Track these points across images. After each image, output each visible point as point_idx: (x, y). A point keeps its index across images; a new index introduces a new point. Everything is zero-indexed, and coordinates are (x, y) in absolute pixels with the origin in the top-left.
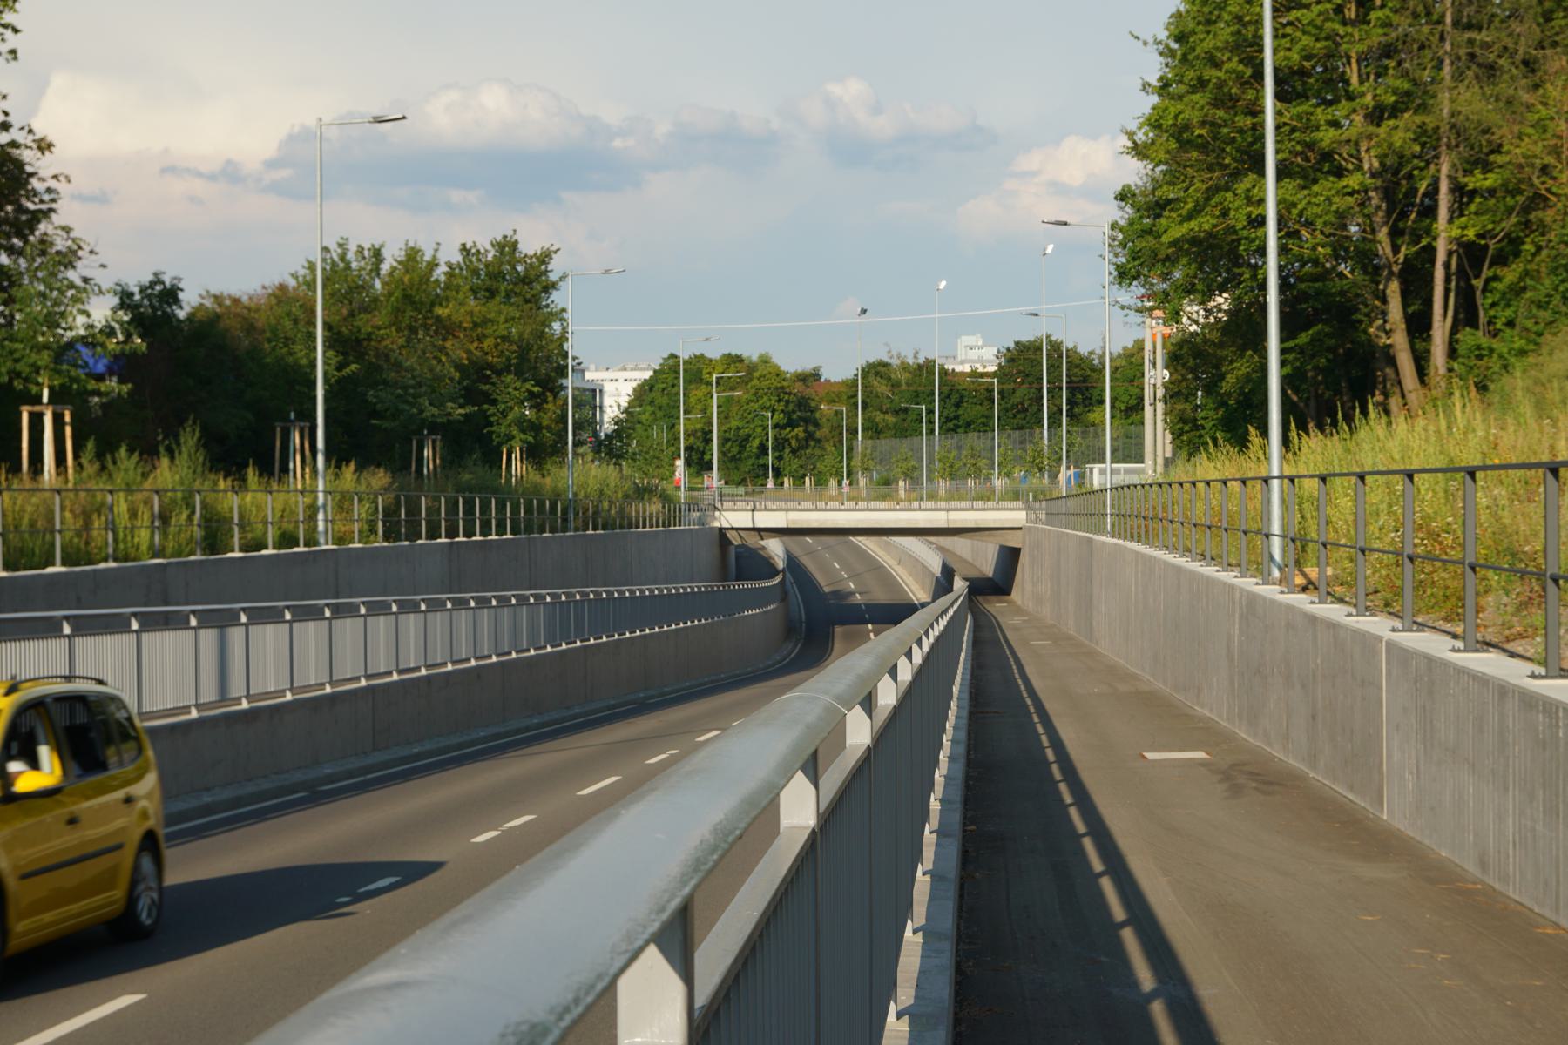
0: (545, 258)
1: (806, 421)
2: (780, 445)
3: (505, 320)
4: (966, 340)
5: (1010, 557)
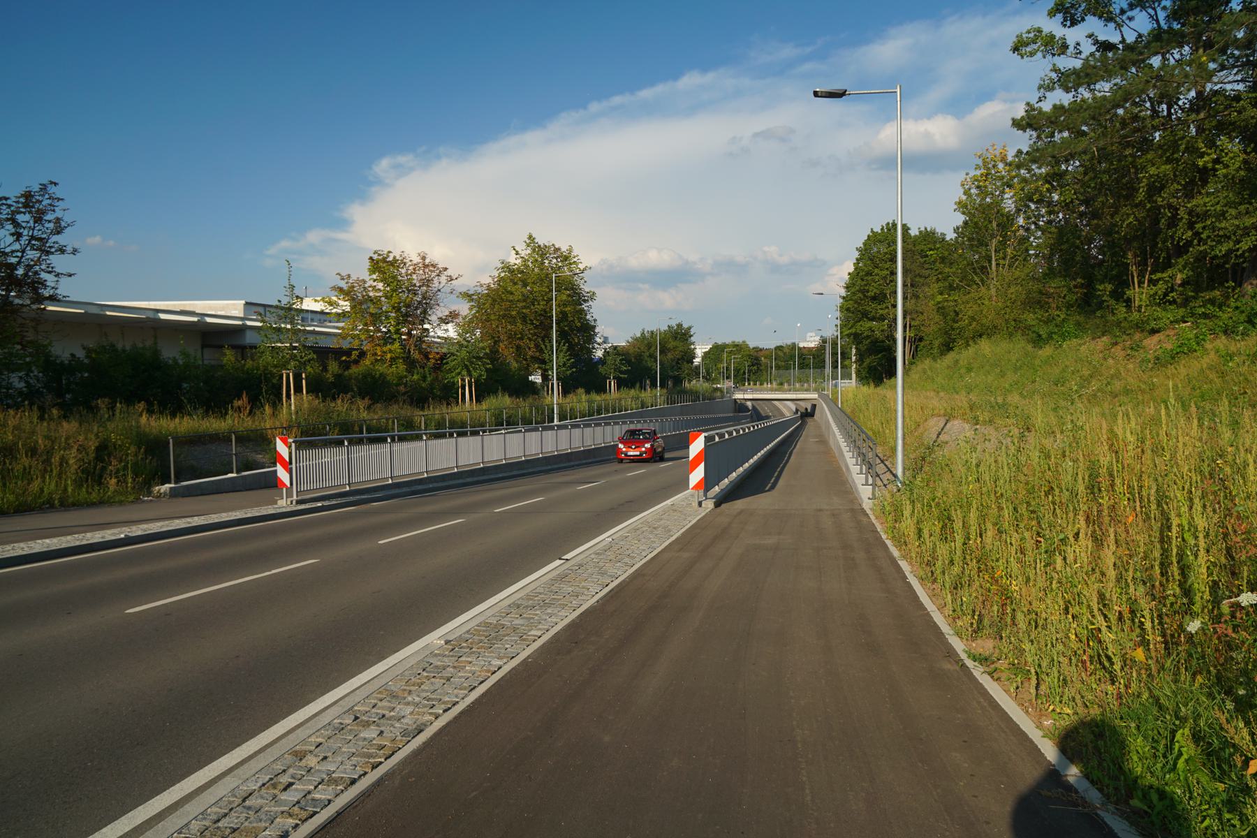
0: (690, 328)
1: (757, 364)
2: (750, 371)
4: (810, 334)
5: (814, 406)
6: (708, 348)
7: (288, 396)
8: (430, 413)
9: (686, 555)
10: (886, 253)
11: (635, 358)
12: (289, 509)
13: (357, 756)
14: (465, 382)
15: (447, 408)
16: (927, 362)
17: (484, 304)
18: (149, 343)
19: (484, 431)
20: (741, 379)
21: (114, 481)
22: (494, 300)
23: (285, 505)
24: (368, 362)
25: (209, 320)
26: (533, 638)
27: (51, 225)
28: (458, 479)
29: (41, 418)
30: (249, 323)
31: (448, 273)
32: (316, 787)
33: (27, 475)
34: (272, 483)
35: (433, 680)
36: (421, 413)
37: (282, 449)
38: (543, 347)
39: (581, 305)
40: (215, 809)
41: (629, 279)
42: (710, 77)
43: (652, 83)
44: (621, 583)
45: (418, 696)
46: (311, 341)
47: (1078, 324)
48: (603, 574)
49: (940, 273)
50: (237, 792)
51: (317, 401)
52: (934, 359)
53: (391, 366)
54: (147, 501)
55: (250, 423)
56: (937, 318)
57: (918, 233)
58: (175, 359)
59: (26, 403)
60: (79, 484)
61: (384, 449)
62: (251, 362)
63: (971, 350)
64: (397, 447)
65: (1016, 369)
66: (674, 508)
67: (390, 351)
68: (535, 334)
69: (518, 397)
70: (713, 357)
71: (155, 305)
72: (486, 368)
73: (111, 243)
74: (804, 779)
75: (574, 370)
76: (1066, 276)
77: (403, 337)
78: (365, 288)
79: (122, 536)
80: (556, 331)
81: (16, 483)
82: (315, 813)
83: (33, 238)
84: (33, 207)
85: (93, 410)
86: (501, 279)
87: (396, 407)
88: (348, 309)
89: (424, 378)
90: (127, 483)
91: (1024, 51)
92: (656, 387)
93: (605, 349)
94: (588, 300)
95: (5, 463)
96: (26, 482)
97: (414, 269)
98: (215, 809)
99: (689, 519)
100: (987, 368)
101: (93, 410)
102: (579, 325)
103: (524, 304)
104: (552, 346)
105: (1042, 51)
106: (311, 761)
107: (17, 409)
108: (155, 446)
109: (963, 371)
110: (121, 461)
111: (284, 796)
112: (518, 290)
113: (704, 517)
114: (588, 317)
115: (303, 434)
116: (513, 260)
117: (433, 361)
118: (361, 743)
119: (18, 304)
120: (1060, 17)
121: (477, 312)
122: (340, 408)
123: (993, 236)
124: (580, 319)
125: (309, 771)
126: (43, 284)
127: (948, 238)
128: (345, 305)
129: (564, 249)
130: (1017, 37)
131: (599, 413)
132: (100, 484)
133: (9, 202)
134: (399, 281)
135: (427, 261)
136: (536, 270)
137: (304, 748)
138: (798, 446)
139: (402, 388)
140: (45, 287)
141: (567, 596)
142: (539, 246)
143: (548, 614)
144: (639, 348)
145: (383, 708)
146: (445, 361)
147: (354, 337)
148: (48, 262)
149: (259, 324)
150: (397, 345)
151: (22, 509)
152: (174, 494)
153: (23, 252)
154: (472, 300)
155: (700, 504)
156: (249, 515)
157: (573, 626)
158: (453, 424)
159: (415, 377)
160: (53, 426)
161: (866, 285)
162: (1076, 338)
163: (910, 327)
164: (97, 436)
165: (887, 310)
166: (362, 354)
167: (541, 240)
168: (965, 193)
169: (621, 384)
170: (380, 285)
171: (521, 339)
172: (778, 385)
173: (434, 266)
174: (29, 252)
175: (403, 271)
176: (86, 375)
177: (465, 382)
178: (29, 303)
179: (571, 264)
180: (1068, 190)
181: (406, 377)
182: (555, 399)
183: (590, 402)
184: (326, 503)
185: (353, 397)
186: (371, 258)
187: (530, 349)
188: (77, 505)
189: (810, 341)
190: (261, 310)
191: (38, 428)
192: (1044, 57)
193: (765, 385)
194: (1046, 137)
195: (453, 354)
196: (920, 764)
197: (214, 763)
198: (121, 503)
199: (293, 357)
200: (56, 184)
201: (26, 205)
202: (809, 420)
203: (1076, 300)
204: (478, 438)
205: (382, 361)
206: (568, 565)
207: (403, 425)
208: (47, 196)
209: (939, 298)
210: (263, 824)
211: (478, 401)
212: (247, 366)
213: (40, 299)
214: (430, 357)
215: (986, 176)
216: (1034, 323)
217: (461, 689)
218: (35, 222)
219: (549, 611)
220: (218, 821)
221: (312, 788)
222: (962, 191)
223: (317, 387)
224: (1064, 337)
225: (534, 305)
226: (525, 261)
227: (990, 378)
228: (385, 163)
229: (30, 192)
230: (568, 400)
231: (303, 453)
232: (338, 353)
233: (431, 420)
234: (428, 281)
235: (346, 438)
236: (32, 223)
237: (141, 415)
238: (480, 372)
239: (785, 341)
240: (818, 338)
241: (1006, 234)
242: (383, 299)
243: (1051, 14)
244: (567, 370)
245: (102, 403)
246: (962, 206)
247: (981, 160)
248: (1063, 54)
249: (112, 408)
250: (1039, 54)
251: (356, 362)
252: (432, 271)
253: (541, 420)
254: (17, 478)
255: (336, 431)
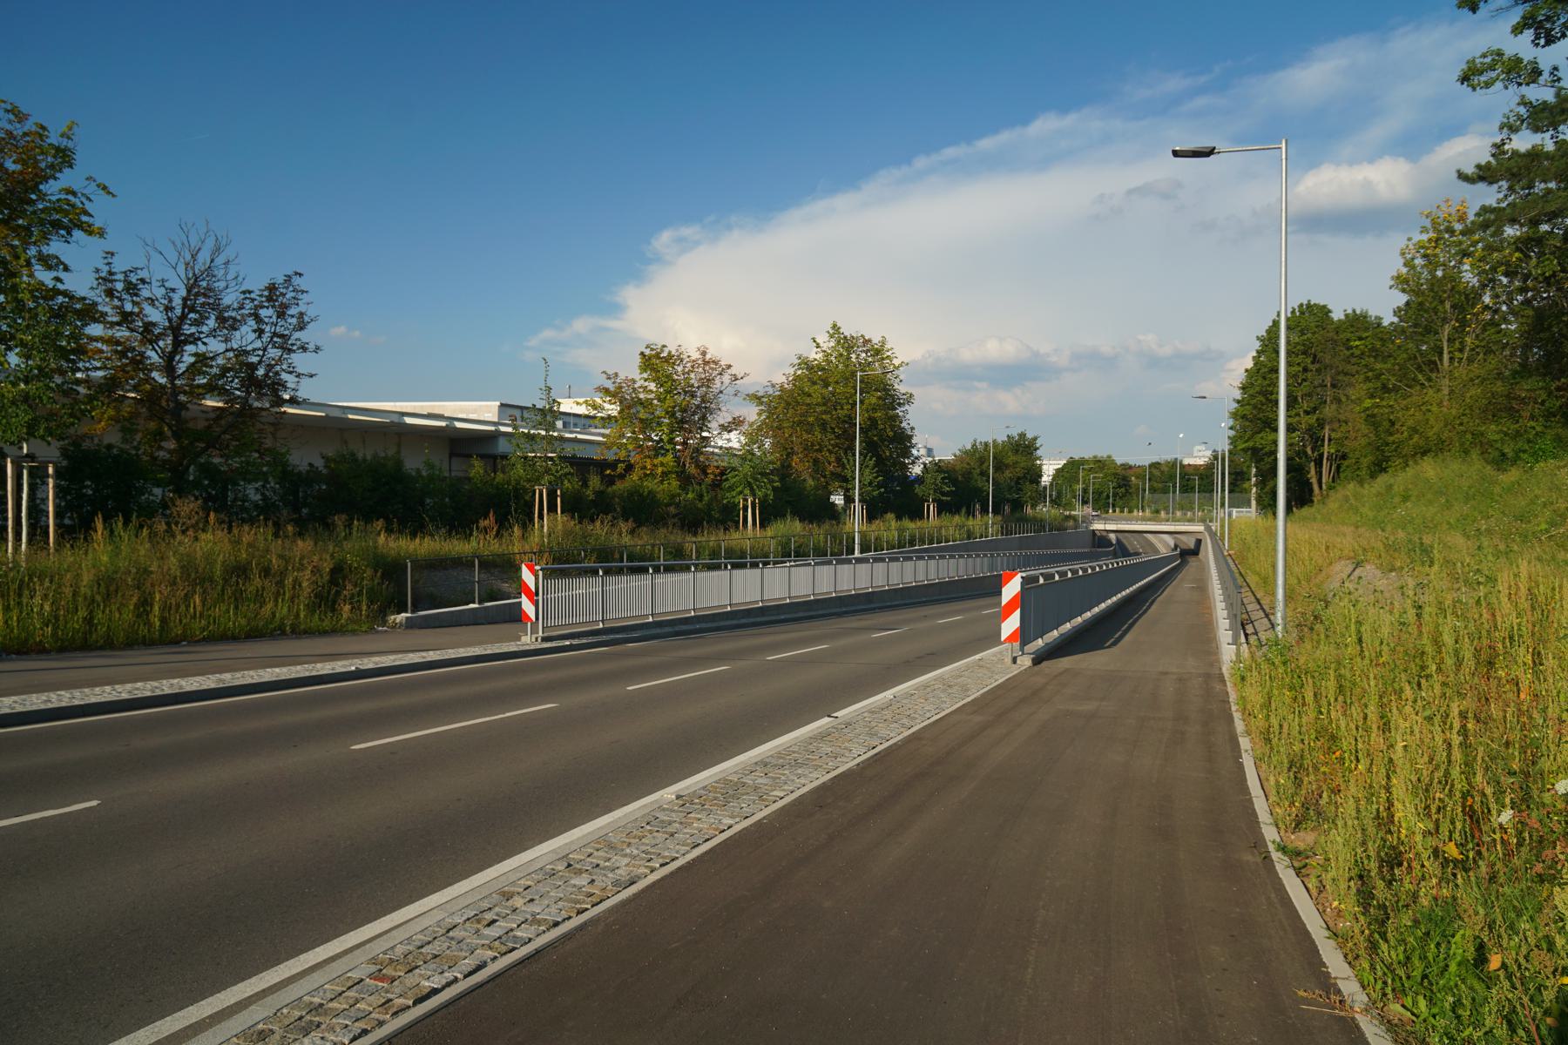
0: (1035, 439)
1: (1125, 485)
2: (1115, 495)
3: (1023, 462)
5: (1199, 542)
6: (1060, 463)
7: (541, 517)
8: (704, 539)
9: (977, 719)
10: (1298, 343)
11: (963, 475)
12: (532, 647)
13: (565, 901)
14: (748, 504)
15: (725, 534)
16: (1351, 486)
17: (776, 408)
18: (391, 452)
19: (765, 564)
20: (1102, 503)
21: (347, 607)
22: (788, 404)
23: (529, 642)
24: (635, 478)
25: (459, 425)
26: (774, 798)
27: (294, 321)
28: (732, 619)
29: (276, 535)
30: (503, 429)
31: (732, 371)
32: (518, 926)
33: (259, 598)
34: (515, 616)
35: (656, 834)
36: (694, 539)
37: (527, 576)
38: (846, 462)
39: (896, 409)
40: (419, 937)
41: (961, 375)
42: (1070, 120)
43: (995, 130)
44: (891, 746)
45: (637, 849)
46: (569, 450)
47: (1558, 439)
48: (872, 735)
49: (1371, 370)
50: (442, 924)
51: (573, 523)
52: (1361, 483)
53: (662, 482)
54: (381, 631)
55: (497, 546)
56: (1364, 429)
57: (1343, 317)
58: (418, 471)
59: (262, 517)
60: (311, 609)
61: (644, 581)
62: (501, 476)
63: (1410, 471)
64: (661, 579)
65: (1467, 498)
66: (981, 663)
67: (662, 464)
68: (836, 445)
69: (811, 522)
70: (1066, 475)
71: (401, 407)
72: (773, 487)
73: (357, 333)
74: (1031, 958)
75: (883, 490)
76: (1545, 375)
77: (678, 447)
78: (634, 389)
79: (353, 668)
80: (860, 442)
81: (248, 606)
82: (514, 949)
83: (275, 334)
84: (277, 300)
85: (329, 527)
86: (797, 378)
87: (663, 531)
88: (615, 413)
89: (701, 497)
90: (361, 611)
91: (1476, 82)
92: (988, 512)
93: (925, 464)
94: (904, 404)
95: (238, 583)
96: (258, 605)
97: (693, 367)
98: (419, 937)
99: (997, 677)
100: (1429, 496)
101: (329, 527)
102: (891, 434)
103: (824, 408)
104: (855, 461)
105: (1502, 80)
106: (518, 902)
107: (252, 525)
108: (392, 570)
109: (1397, 500)
110: (355, 585)
111: (487, 931)
112: (817, 392)
113: (1014, 676)
114: (904, 425)
115: (554, 561)
116: (815, 356)
117: (712, 477)
118: (570, 889)
119: (258, 408)
120: (1529, 34)
121: (768, 417)
122: (599, 532)
123: (1445, 320)
124: (892, 427)
125: (514, 911)
126: (284, 385)
127: (1385, 323)
128: (613, 409)
129: (876, 340)
130: (1468, 62)
131: (912, 543)
132: (333, 610)
133: (253, 296)
134: (674, 381)
135: (708, 357)
136: (840, 366)
137: (512, 889)
138: (1165, 593)
139: (672, 510)
140: (285, 388)
141: (825, 757)
142: (845, 337)
143: (797, 775)
144: (968, 464)
145: (598, 858)
146: (724, 477)
147: (621, 446)
148: (290, 361)
149: (510, 430)
150: (670, 456)
151: (254, 634)
152: (410, 624)
153: (265, 350)
154: (761, 403)
155: (1014, 660)
156: (489, 652)
157: (823, 788)
158: (730, 553)
159: (690, 496)
160: (287, 542)
161: (1269, 385)
162: (1555, 458)
163: (1330, 440)
164: (332, 556)
165: (1297, 418)
166: (630, 468)
167: (847, 331)
168: (1405, 265)
169: (943, 508)
170: (652, 386)
171: (820, 450)
172: (1152, 513)
173: (715, 363)
174: (270, 351)
175: (680, 369)
176: (324, 487)
177: (748, 504)
178: (268, 406)
179: (883, 359)
180: (1548, 259)
181: (679, 495)
182: (856, 523)
183: (901, 530)
184: (575, 642)
185: (614, 518)
186: (642, 354)
187: (830, 464)
188: (309, 633)
189: (1198, 457)
190: (517, 413)
191: (272, 547)
192: (1506, 88)
193: (1135, 513)
194: (1523, 189)
195: (734, 469)
196: (1168, 955)
197: (426, 899)
198: (354, 632)
199: (548, 471)
200: (300, 275)
201: (269, 299)
202: (1192, 560)
203: (1561, 407)
204: (757, 572)
205: (653, 475)
206: (838, 721)
207: (671, 553)
208: (291, 289)
209: (1368, 403)
210: (464, 954)
211: (763, 526)
212: (497, 480)
213: (281, 402)
214: (709, 471)
215: (1436, 241)
216: (1497, 437)
217: (683, 845)
218: (278, 317)
219: (799, 771)
220: (422, 947)
221: (515, 926)
222: (1402, 261)
223: (576, 507)
224: (1537, 456)
225: (836, 410)
226: (827, 355)
227: (1432, 510)
228: (666, 236)
229: (274, 284)
230: (874, 527)
231: (552, 583)
232: (602, 465)
233: (704, 548)
234: (708, 380)
235: (601, 567)
236: (274, 319)
237: (379, 534)
238: (765, 491)
239: (1163, 455)
240: (1209, 453)
241: (1465, 317)
242: (655, 402)
243: (1517, 30)
244: (873, 491)
245: (340, 520)
246: (1401, 282)
247: (1429, 220)
248: (1534, 82)
249: (349, 526)
250: (1499, 85)
251: (622, 477)
252: (713, 369)
253: (839, 551)
254: (248, 600)
255: (593, 559)
